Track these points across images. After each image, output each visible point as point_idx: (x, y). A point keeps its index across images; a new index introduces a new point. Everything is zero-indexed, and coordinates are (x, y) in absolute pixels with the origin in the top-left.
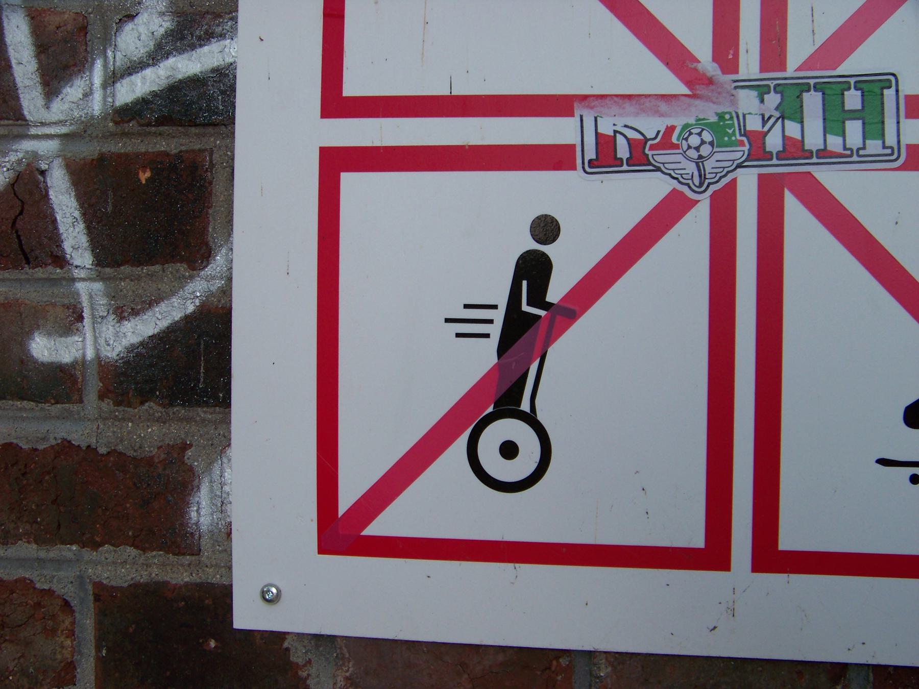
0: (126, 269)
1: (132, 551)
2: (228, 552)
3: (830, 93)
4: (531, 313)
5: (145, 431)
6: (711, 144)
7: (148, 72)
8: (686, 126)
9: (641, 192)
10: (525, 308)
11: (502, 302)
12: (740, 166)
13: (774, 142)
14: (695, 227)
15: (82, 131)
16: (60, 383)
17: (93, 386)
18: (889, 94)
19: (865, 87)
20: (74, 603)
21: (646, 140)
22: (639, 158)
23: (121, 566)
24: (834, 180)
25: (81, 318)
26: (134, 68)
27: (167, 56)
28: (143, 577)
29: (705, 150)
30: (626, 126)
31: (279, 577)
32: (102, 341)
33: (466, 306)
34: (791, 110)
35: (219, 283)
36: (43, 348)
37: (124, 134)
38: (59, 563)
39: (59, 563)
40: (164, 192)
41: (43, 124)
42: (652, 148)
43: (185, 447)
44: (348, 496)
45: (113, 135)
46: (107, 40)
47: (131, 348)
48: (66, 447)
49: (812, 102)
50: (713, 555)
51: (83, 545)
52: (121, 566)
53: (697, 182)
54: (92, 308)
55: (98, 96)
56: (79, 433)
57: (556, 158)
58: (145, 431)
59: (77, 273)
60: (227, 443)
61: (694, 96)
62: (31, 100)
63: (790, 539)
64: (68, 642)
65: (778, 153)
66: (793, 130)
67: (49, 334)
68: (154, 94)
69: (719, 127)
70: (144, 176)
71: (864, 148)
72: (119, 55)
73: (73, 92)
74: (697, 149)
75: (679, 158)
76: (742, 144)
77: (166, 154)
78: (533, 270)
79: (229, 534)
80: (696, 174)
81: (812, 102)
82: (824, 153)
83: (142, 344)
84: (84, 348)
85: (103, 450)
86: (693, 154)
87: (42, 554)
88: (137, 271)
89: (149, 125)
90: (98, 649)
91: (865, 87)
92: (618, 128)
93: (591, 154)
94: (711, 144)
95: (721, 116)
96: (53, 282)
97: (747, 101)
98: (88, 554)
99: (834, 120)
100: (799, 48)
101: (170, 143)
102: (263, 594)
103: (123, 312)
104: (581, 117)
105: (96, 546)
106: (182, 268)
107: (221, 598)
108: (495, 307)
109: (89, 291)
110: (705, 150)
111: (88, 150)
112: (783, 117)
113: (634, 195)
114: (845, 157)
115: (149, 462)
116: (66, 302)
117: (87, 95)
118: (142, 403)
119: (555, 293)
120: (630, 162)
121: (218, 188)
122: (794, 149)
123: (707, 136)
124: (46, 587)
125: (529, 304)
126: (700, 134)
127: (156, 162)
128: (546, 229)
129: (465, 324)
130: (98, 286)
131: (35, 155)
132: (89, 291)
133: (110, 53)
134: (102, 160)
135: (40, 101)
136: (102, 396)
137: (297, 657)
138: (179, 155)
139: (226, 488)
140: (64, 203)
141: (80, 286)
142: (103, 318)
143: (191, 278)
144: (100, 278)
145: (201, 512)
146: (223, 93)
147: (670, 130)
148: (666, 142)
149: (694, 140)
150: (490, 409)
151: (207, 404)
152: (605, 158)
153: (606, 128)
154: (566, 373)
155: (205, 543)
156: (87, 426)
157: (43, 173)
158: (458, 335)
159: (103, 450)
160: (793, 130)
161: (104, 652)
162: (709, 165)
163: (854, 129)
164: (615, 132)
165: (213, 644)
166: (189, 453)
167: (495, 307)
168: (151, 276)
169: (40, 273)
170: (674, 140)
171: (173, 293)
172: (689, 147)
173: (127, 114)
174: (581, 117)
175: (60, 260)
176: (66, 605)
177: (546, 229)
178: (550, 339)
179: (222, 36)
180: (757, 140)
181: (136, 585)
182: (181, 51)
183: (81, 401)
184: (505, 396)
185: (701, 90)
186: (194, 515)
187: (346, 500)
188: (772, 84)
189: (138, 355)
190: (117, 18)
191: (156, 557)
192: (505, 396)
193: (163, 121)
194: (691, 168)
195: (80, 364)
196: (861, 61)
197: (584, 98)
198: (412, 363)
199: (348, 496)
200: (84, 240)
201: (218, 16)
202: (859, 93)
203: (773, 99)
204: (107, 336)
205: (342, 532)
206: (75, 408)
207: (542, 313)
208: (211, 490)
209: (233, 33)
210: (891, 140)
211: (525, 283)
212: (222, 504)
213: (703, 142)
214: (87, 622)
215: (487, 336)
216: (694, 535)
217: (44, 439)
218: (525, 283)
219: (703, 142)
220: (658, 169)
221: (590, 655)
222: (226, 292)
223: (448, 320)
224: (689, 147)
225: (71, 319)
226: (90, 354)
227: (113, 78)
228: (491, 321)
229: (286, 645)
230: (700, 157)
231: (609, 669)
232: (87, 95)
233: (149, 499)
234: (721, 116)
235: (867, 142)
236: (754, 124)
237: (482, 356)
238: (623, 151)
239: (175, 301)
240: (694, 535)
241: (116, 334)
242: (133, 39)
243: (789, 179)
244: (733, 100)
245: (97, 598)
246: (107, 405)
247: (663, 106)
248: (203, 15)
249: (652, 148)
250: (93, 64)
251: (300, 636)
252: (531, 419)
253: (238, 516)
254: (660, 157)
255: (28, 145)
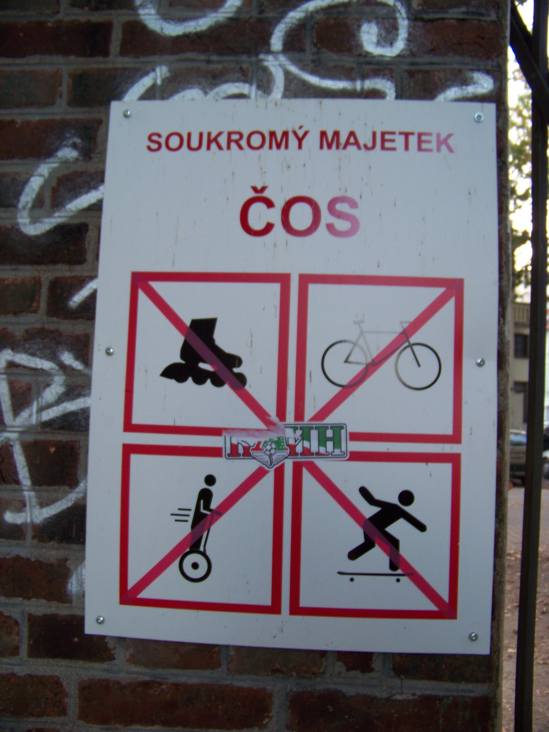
0: (44, 487)
1: (43, 601)
2: (83, 603)
3: (321, 430)
4: (204, 513)
5: (51, 553)
6: (275, 449)
7: (55, 408)
8: (265, 442)
9: (248, 467)
10: (202, 511)
11: (193, 507)
12: (286, 458)
13: (299, 449)
14: (269, 480)
15: (27, 431)
16: (16, 532)
17: (29, 534)
18: (343, 431)
19: (335, 429)
20: (20, 621)
21: (250, 447)
22: (247, 453)
23: (40, 607)
24: (321, 464)
25: (25, 505)
26: (49, 406)
27: (62, 402)
28: (48, 611)
29: (273, 451)
30: (242, 441)
31: (104, 614)
32: (34, 516)
33: (180, 509)
34: (306, 436)
35: (81, 495)
36: (10, 517)
37: (45, 433)
38: (14, 605)
39: (14, 605)
40: (60, 457)
41: (12, 427)
42: (253, 450)
43: (66, 560)
44: (132, 582)
45: (40, 433)
46: (39, 394)
47: (46, 519)
48: (18, 558)
49: (314, 434)
50: (274, 608)
51: (24, 598)
52: (40, 607)
53: (269, 463)
54: (30, 502)
55: (34, 417)
56: (24, 553)
57: (215, 452)
58: (51, 553)
59: (24, 488)
60: (83, 558)
61: (268, 430)
62: (8, 417)
63: (304, 602)
64: (17, 638)
65: (328, 429)
66: (306, 444)
67: (12, 512)
68: (57, 418)
69: (278, 443)
70: (52, 450)
71: (334, 452)
72: (44, 401)
73: (25, 414)
74: (270, 451)
75: (263, 454)
76: (287, 449)
77: (61, 442)
78: (205, 496)
79: (84, 596)
80: (269, 460)
81: (314, 434)
82: (318, 454)
83: (50, 518)
84: (26, 518)
85: (33, 560)
86: (268, 453)
87: (7, 601)
88: (49, 488)
89: (55, 429)
90: (29, 640)
91: (335, 429)
92: (240, 441)
93: (228, 451)
94: (275, 449)
95: (279, 438)
96: (15, 491)
97: (289, 433)
98: (26, 602)
99: (322, 441)
100: (309, 412)
101: (63, 437)
102: (97, 620)
103: (43, 504)
104: (225, 437)
105: (29, 598)
106: (67, 488)
107: (80, 621)
108: (190, 510)
109: (29, 495)
110: (273, 451)
111: (30, 438)
112: (303, 439)
113: (246, 467)
114: (326, 455)
115: (52, 565)
116: (20, 499)
117: (30, 416)
118: (50, 541)
119: (214, 505)
120: (244, 455)
121: (82, 456)
122: (307, 452)
123: (274, 446)
124: (8, 614)
125: (204, 509)
126: (271, 445)
127: (57, 444)
128: (210, 480)
129: (178, 516)
130: (32, 494)
131: (8, 439)
132: (29, 495)
133: (40, 400)
134: (35, 443)
135: (11, 417)
136: (33, 538)
137: (111, 645)
138: (67, 443)
139: (83, 577)
140: (20, 459)
141: (26, 493)
142: (34, 506)
143: (70, 492)
144: (33, 490)
145: (73, 586)
146: (85, 419)
147: (259, 443)
148: (257, 448)
149: (268, 447)
150: (188, 550)
151: (75, 543)
152: (234, 452)
153: (235, 441)
154: (217, 536)
155: (74, 598)
156: (27, 549)
157: (11, 446)
158: (176, 520)
159: (33, 560)
160: (306, 444)
161: (31, 642)
162: (274, 457)
163: (330, 445)
164: (238, 443)
165: (76, 640)
166: (68, 562)
167: (190, 510)
168: (54, 490)
169: (9, 487)
170: (261, 446)
171: (63, 498)
172: (267, 450)
173: (46, 425)
174: (225, 437)
175: (17, 482)
176: (16, 623)
177: (210, 480)
178: (212, 522)
179: (85, 396)
180: (292, 448)
181: (45, 615)
182: (68, 400)
183: (24, 539)
184: (194, 544)
185: (272, 428)
186: (69, 587)
187: (131, 584)
188: (299, 426)
189: (49, 522)
190: (43, 385)
191: (54, 604)
192: (194, 544)
193: (62, 428)
194: (267, 458)
195: (24, 525)
196: (332, 419)
197: (226, 429)
198: (158, 531)
199: (132, 582)
200: (27, 475)
201: (83, 387)
202: (332, 431)
203: (299, 432)
204: (36, 513)
205: (129, 596)
206: (21, 542)
207: (208, 513)
208: (77, 577)
209: (88, 394)
210: (344, 449)
211: (202, 501)
212: (81, 583)
213: (272, 448)
214: (25, 630)
215: (186, 521)
216: (267, 601)
217: (9, 554)
218: (202, 501)
219: (272, 448)
220: (254, 458)
221: (227, 647)
222: (84, 498)
223: (172, 514)
224: (267, 450)
225: (21, 506)
226: (29, 520)
227: (41, 410)
228: (188, 515)
229: (106, 640)
230: (271, 454)
231: (234, 652)
232: (30, 416)
233: (53, 580)
234: (279, 438)
235: (335, 450)
236: (292, 442)
237: (185, 529)
238: (241, 450)
239: (64, 501)
240: (267, 601)
241: (40, 513)
242: (51, 393)
243: (304, 465)
244: (284, 432)
245: (29, 620)
246: (35, 542)
247: (257, 434)
248: (78, 386)
249: (253, 450)
250: (33, 403)
251: (112, 637)
252: (204, 554)
253: (88, 589)
254: (255, 454)
255: (6, 435)
